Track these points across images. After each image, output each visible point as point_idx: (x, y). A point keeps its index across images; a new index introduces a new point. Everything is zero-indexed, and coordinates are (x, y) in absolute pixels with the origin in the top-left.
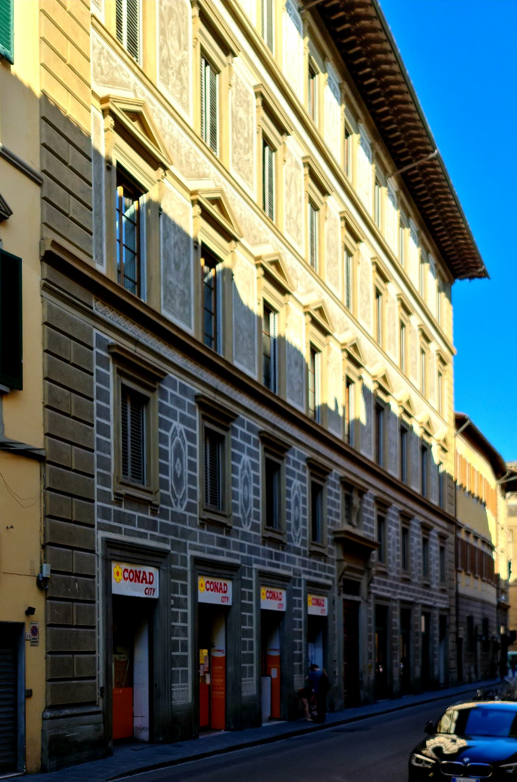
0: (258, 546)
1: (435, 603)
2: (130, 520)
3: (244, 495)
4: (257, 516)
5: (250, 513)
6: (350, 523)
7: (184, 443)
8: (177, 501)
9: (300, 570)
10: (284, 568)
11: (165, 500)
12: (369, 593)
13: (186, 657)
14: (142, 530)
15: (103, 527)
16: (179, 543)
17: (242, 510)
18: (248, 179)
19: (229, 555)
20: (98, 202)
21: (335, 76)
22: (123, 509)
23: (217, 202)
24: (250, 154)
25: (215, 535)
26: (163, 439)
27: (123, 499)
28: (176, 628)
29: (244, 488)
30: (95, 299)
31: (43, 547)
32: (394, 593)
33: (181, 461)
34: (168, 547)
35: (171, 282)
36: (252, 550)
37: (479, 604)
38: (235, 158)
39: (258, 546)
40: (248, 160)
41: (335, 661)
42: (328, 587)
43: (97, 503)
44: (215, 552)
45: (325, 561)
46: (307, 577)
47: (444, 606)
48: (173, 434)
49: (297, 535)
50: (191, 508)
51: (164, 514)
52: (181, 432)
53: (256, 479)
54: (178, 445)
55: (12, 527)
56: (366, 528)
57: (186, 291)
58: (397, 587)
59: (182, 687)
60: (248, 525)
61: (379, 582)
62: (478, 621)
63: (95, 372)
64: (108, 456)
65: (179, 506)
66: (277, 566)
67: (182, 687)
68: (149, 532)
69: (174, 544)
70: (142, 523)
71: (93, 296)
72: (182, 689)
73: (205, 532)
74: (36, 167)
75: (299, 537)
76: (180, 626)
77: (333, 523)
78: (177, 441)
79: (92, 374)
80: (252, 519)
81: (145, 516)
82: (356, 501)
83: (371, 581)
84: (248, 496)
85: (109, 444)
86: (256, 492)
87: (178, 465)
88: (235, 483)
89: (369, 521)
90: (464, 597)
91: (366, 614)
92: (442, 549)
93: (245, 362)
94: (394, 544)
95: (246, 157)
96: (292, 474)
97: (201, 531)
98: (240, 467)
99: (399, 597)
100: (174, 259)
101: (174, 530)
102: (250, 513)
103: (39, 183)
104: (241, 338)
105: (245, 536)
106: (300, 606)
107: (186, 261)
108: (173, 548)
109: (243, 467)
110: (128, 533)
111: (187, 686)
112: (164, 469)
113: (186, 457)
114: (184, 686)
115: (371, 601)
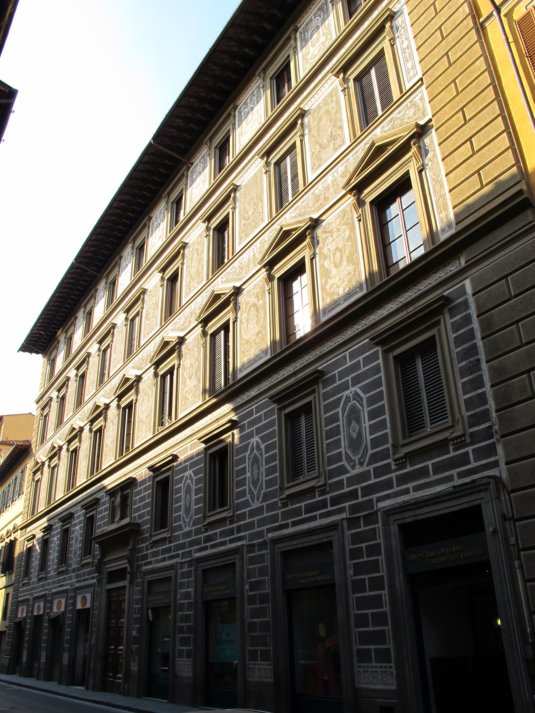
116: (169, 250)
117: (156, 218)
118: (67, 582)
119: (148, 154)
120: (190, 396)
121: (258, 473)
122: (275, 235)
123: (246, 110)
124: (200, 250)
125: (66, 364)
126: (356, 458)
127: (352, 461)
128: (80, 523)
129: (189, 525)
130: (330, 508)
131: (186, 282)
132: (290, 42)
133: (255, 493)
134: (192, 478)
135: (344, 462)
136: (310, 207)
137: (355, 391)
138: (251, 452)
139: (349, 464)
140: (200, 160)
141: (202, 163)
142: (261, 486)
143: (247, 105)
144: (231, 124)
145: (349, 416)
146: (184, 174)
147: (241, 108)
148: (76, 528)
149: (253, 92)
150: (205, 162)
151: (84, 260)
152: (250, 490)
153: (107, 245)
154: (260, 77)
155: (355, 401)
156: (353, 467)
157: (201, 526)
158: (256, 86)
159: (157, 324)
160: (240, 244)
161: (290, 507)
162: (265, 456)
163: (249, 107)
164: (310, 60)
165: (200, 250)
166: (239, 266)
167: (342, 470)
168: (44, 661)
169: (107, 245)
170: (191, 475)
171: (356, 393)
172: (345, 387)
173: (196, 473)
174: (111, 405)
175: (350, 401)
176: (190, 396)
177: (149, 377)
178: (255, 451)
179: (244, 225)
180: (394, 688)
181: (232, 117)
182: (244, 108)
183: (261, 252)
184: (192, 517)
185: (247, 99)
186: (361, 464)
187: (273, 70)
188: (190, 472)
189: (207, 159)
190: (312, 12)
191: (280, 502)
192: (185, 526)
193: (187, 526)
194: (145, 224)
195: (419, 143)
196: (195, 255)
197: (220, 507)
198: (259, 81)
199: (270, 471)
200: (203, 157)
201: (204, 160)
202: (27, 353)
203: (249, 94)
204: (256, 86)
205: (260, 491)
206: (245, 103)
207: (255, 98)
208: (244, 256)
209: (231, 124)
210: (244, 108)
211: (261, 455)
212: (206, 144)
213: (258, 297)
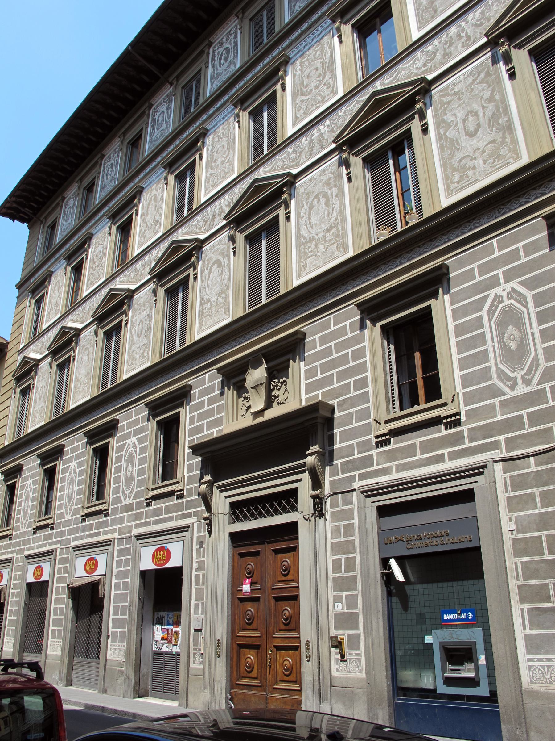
2: (411, 450)
44: (41, 546)
46: (73, 544)
59: (119, 646)
116: (72, 242)
117: (109, 157)
118: (31, 545)
119: (20, 190)
120: (137, 357)
121: (72, 492)
122: (57, 332)
123: (220, 50)
124: (159, 198)
125: (46, 256)
126: (518, 375)
127: (509, 378)
128: (33, 476)
129: (130, 498)
130: (467, 445)
131: (141, 230)
132: (202, 56)
133: (69, 507)
134: (136, 446)
135: (496, 381)
136: (131, 278)
137: (512, 288)
138: (70, 474)
139: (505, 384)
140: (164, 99)
141: (166, 102)
142: (73, 503)
143: (110, 159)
144: (204, 63)
145: (127, 460)
146: (145, 112)
147: (215, 47)
148: (27, 482)
149: (116, 149)
150: (170, 101)
151: (15, 205)
152: (66, 505)
153: (32, 204)
154: (238, 17)
155: (512, 301)
156: (512, 388)
157: (143, 499)
158: (234, 24)
159: (103, 273)
160: (205, 195)
161: (87, 523)
162: (78, 479)
163: (224, 48)
164: (154, 141)
165: (159, 198)
166: (202, 219)
167: (495, 392)
168: (484, 663)
169: (32, 204)
170: (134, 443)
171: (513, 290)
172: (494, 283)
173: (80, 465)
174: (206, 248)
175: (502, 302)
176: (137, 357)
177: (91, 332)
178: (72, 473)
179: (211, 174)
180: (124, 660)
181: (146, 116)
182: (219, 47)
183: (229, 205)
184: (27, 520)
185: (223, 38)
186: (528, 382)
187: (130, 136)
188: (134, 439)
189: (172, 98)
190: (224, 32)
191: (145, 501)
192: (125, 499)
193: (127, 499)
194: (58, 204)
195: (290, 191)
196: (153, 202)
197: (427, 401)
198: (236, 22)
199: (141, 472)
200: (167, 96)
201: (169, 99)
202: (7, 219)
203: (225, 33)
204: (234, 24)
205: (72, 506)
206: (219, 42)
207: (233, 37)
208: (209, 209)
209: (204, 63)
210: (219, 47)
211: (76, 477)
212: (119, 137)
213: (223, 254)
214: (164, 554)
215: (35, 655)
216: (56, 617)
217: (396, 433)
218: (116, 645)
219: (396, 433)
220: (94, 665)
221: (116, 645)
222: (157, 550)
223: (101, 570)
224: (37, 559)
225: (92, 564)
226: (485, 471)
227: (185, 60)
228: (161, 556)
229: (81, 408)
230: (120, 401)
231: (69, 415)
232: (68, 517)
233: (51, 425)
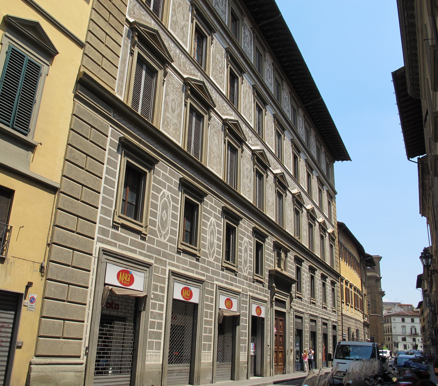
0: (108, 229)
1: (330, 317)
2: (124, 240)
3: (210, 240)
4: (218, 253)
5: (214, 250)
6: (279, 266)
7: (170, 203)
8: (162, 235)
9: (247, 289)
10: (236, 286)
11: (153, 233)
12: (291, 307)
13: (161, 333)
14: (133, 248)
15: (100, 240)
16: (161, 260)
17: (208, 248)
18: (221, 84)
19: (197, 273)
20: (123, 66)
21: (234, 5)
22: (224, 273)
23: (200, 87)
24: (223, 74)
25: (189, 260)
26: (156, 198)
27: (120, 226)
28: (154, 313)
29: (211, 236)
30: (114, 112)
31: (48, 245)
32: (306, 310)
33: (167, 212)
34: (152, 261)
35: (168, 117)
36: (214, 273)
37: (354, 321)
38: (213, 73)
39: (108, 229)
40: (222, 77)
41: (268, 346)
42: (265, 302)
43: (98, 225)
44: (187, 270)
45: (302, 301)
46: (251, 294)
47: (335, 320)
48: (162, 196)
49: (246, 269)
50: (170, 240)
51: (152, 241)
52: (168, 196)
53: (250, 249)
54: (165, 203)
55: (23, 227)
56: (289, 272)
57: (178, 124)
58: (308, 306)
59: (155, 352)
60: (212, 258)
61: (297, 303)
62: (353, 330)
63: (107, 149)
64: (111, 199)
65: (163, 238)
66: (232, 285)
67: (155, 352)
68: (138, 250)
69: (157, 260)
70: (133, 243)
71: (112, 109)
72: (155, 354)
73: (224, 273)
74: (83, 40)
75: (246, 270)
76: (157, 313)
77: (269, 266)
78: (165, 201)
79: (105, 150)
80: (215, 255)
81: (137, 240)
82: (283, 255)
83: (291, 300)
84: (213, 241)
85: (114, 191)
86: (218, 239)
87: (164, 214)
88: (205, 232)
89: (291, 267)
90: (346, 316)
91: (290, 320)
92: (333, 290)
93: (215, 169)
94: (319, 289)
95: (220, 75)
96: (244, 234)
97: (179, 256)
98: (209, 224)
99: (321, 316)
100: (172, 106)
101: (158, 252)
102: (214, 250)
103: (81, 45)
104: (213, 156)
105: (210, 263)
106: (246, 310)
107: (179, 110)
108: (155, 263)
109: (211, 224)
110: (141, 254)
111: (159, 353)
112: (154, 215)
113: (171, 211)
114: (157, 352)
115: (292, 312)
214: (128, 277)
215: (176, 365)
216: (206, 334)
217: (124, 227)
218: (153, 352)
219: (124, 227)
220: (225, 366)
221: (153, 352)
222: (122, 271)
223: (234, 308)
224: (185, 281)
225: (229, 303)
226: (151, 267)
227: (297, 98)
228: (126, 278)
229: (118, 103)
230: (228, 198)
231: (282, 231)
232: (211, 260)
233: (198, 165)
